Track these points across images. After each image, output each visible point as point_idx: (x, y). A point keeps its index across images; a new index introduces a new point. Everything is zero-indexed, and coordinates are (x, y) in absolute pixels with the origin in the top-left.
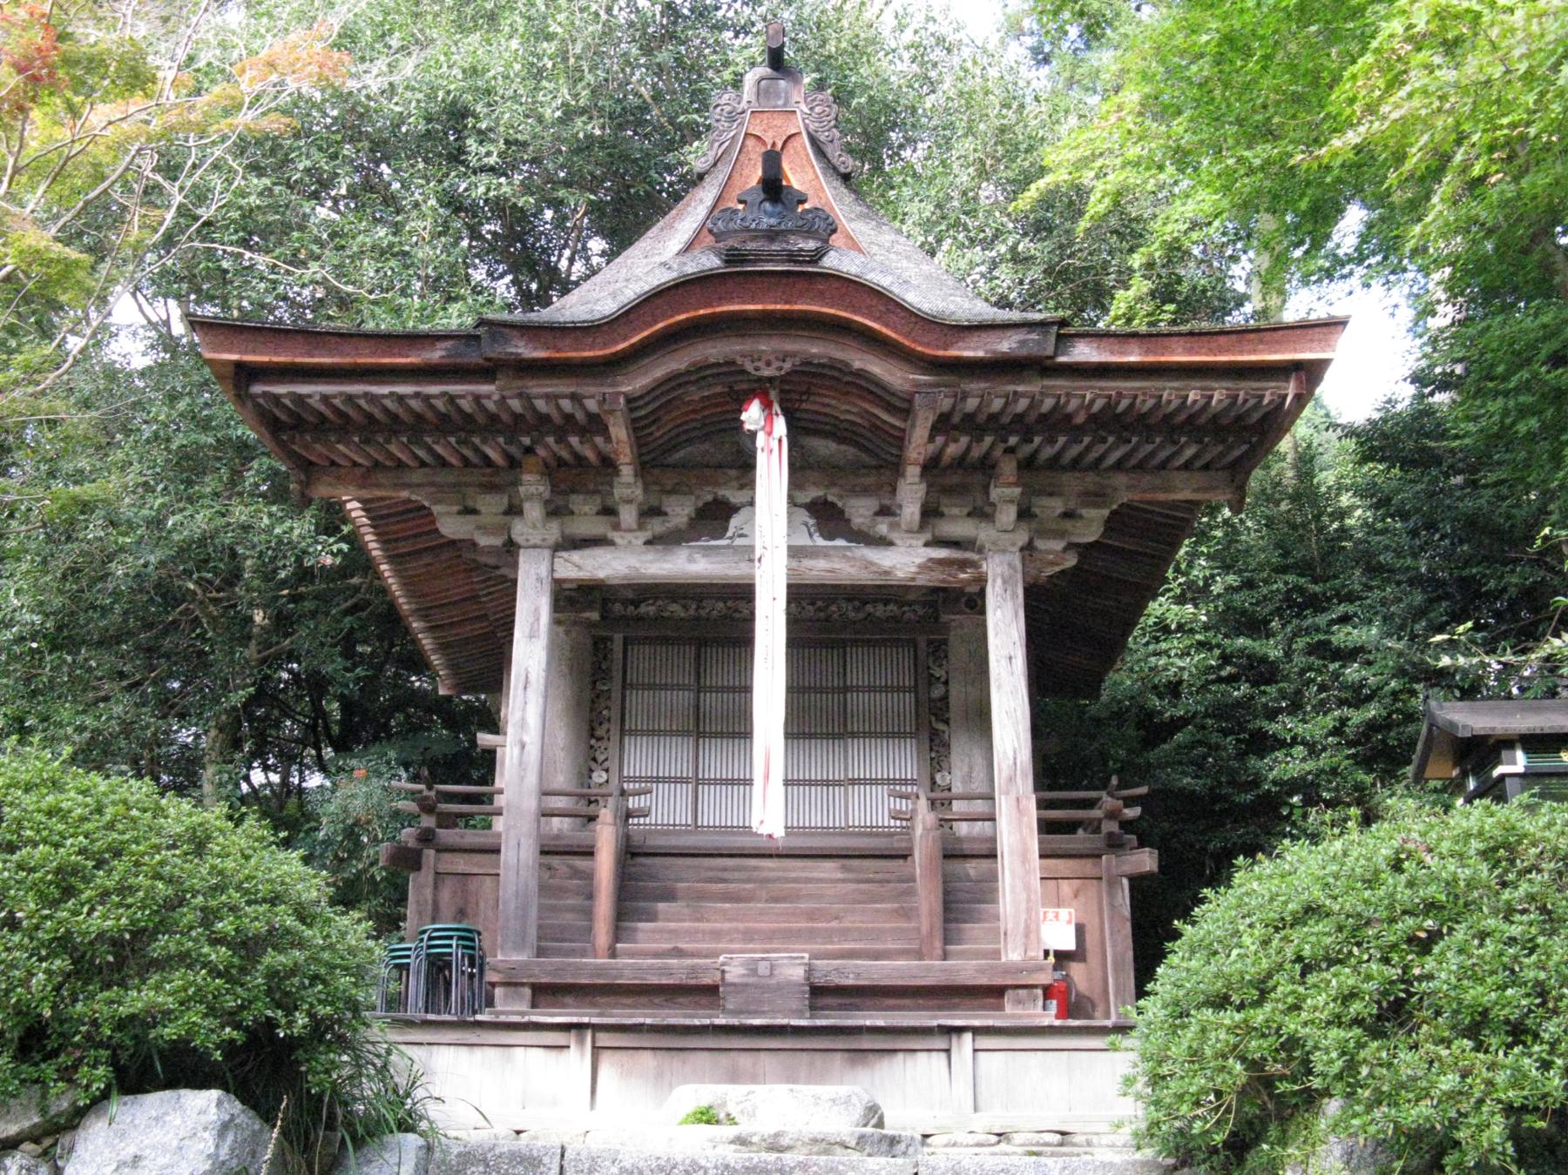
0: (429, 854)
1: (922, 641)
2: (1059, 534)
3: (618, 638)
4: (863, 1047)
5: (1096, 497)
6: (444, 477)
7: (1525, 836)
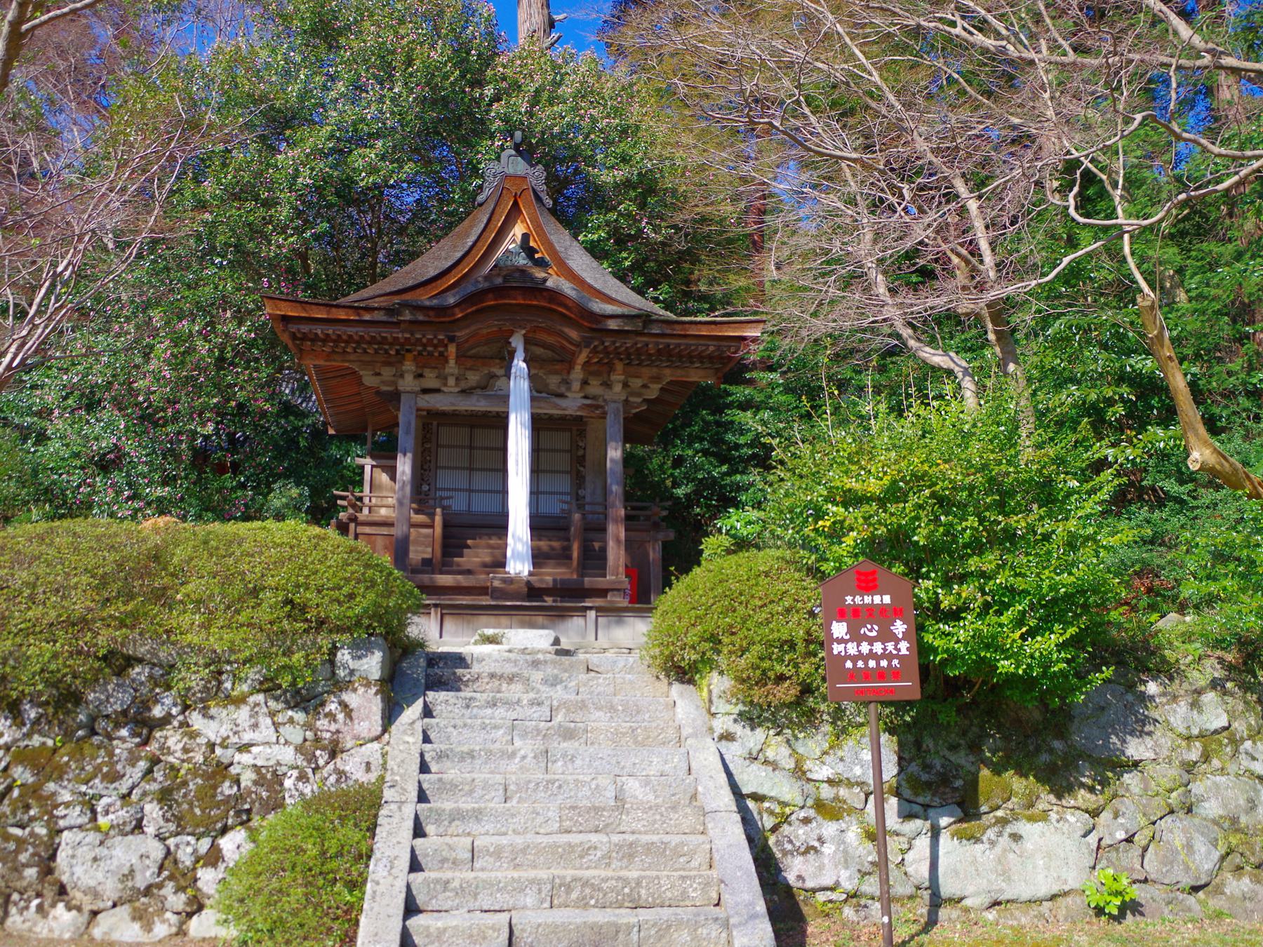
0: (352, 526)
1: (574, 428)
2: (639, 395)
3: (435, 423)
4: (558, 615)
5: (656, 379)
6: (367, 358)
7: (539, 925)
